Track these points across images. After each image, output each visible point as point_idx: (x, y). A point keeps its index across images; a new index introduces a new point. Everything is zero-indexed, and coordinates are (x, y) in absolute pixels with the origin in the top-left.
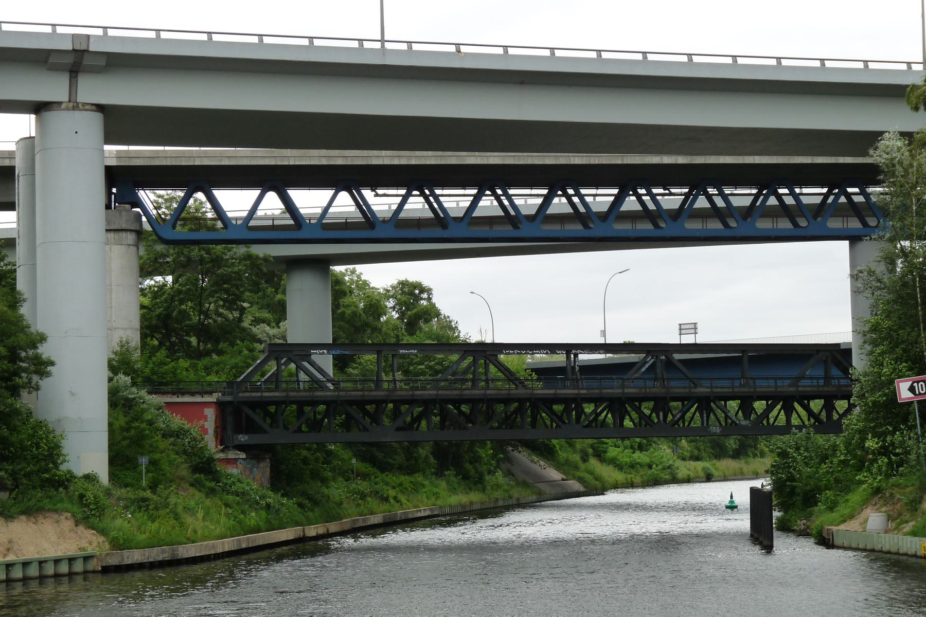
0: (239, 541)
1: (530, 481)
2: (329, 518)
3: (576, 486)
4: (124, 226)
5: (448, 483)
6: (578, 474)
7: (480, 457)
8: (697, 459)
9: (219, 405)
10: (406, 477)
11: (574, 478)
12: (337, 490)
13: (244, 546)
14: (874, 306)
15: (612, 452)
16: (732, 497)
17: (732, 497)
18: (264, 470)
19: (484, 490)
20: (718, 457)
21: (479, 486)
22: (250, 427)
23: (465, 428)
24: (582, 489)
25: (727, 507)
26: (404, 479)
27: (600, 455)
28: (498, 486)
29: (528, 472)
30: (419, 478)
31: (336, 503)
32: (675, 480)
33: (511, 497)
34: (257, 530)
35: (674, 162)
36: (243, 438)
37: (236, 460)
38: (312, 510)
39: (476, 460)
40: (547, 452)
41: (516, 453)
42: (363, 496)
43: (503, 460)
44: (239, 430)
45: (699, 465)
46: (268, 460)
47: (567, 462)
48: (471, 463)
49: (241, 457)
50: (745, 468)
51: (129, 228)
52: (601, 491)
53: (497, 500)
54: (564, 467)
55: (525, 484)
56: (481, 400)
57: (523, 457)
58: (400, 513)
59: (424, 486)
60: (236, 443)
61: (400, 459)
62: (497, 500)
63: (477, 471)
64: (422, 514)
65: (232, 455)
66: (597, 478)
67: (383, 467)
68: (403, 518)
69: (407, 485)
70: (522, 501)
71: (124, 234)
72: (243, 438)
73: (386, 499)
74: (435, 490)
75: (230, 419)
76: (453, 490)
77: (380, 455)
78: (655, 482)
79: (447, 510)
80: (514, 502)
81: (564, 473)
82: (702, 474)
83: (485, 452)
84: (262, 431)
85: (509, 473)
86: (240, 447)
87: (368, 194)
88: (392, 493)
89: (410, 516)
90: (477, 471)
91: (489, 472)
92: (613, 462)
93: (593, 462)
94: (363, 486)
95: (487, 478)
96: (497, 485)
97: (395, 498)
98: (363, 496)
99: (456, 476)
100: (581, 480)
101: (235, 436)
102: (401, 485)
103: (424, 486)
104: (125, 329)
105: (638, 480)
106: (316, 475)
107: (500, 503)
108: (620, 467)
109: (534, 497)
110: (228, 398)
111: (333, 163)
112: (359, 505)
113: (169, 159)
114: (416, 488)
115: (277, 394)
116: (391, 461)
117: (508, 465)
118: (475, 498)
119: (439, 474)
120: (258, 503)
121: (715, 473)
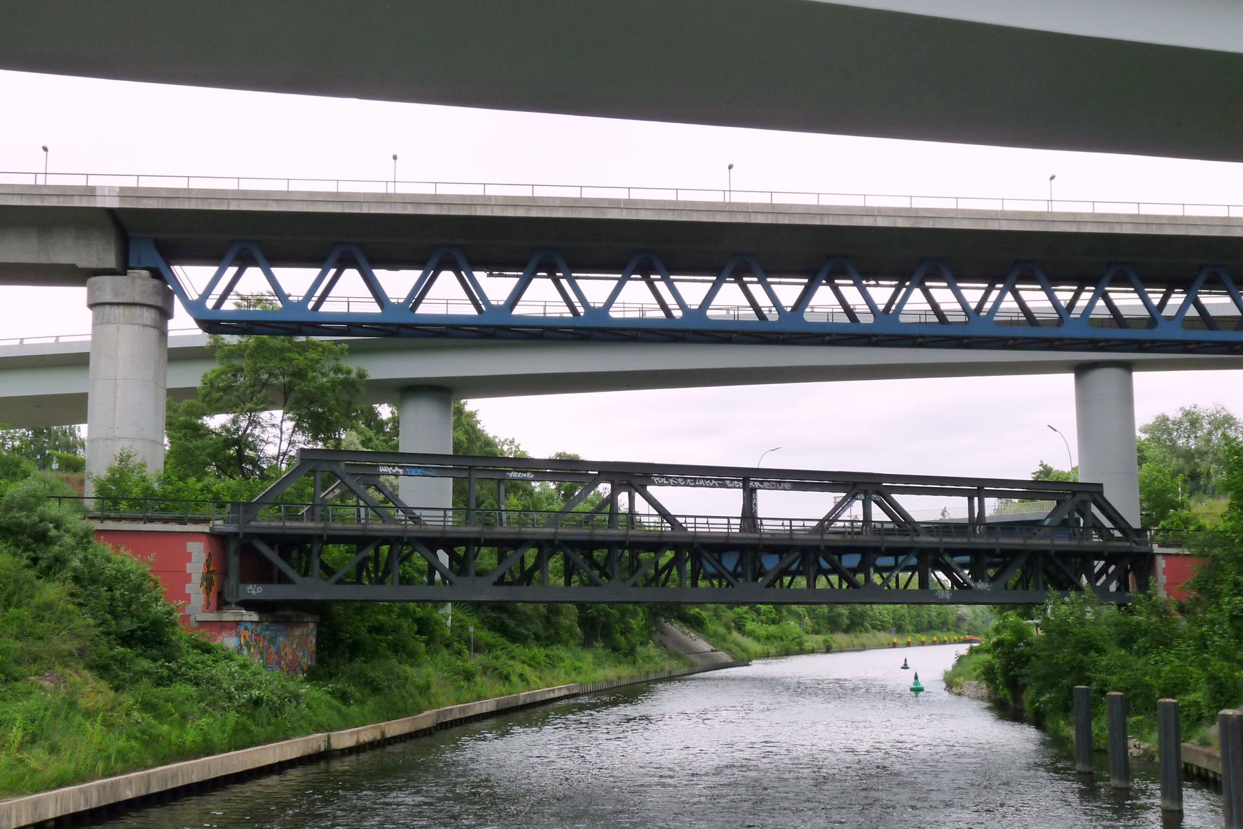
0: (114, 786)
1: (682, 652)
2: (394, 713)
3: (724, 657)
4: (138, 299)
5: (595, 656)
6: (726, 645)
7: (632, 629)
8: (817, 633)
9: (219, 540)
10: (542, 649)
11: (722, 649)
12: (430, 671)
13: (155, 789)
14: (1063, 473)
15: (750, 626)
16: (916, 678)
17: (916, 678)
18: (300, 642)
19: (634, 662)
20: (832, 632)
21: (630, 658)
22: (266, 573)
23: (597, 585)
24: (730, 660)
25: (912, 690)
26: (538, 652)
27: (740, 628)
28: (649, 659)
29: (679, 643)
30: (558, 651)
31: (417, 687)
32: (802, 651)
33: (662, 670)
34: (208, 749)
35: (892, 225)
36: (254, 591)
37: (238, 623)
38: (361, 702)
39: (626, 631)
40: (696, 624)
41: (668, 625)
42: (469, 676)
43: (653, 630)
44: (245, 579)
45: (820, 638)
46: (312, 626)
47: (716, 634)
48: (623, 633)
49: (246, 618)
50: (856, 642)
51: (144, 301)
52: (746, 663)
53: (648, 673)
54: (718, 640)
55: (678, 657)
56: (621, 544)
57: (675, 629)
58: (523, 695)
59: (562, 660)
60: (243, 597)
61: (538, 626)
62: (648, 673)
63: (629, 643)
64: (557, 694)
65: (228, 616)
66: (744, 650)
67: (515, 638)
68: (528, 701)
69: (542, 659)
70: (675, 673)
71: (137, 310)
72: (254, 591)
73: (506, 678)
74: (577, 664)
75: (234, 560)
76: (599, 663)
77: (511, 623)
78: (786, 653)
79: (590, 688)
80: (666, 674)
81: (712, 644)
82: (822, 646)
83: (636, 623)
84: (283, 579)
85: (661, 644)
86: (248, 605)
87: (480, 276)
88: (519, 667)
89: (539, 698)
90: (629, 643)
91: (641, 644)
92: (751, 634)
93: (736, 635)
94: (474, 661)
95: (639, 649)
96: (649, 657)
97: (521, 676)
98: (469, 676)
99: (604, 648)
100: (728, 651)
101: (242, 586)
102: (533, 658)
103: (562, 660)
104: (133, 439)
105: (773, 651)
106: (401, 650)
107: (652, 677)
108: (757, 639)
109: (686, 670)
110: (231, 528)
111: (423, 212)
112: (461, 688)
113: (193, 202)
114: (552, 663)
115: (311, 525)
116: (523, 630)
117: (495, 578)
118: (620, 672)
119: (586, 644)
120: (230, 698)
121: (834, 645)
